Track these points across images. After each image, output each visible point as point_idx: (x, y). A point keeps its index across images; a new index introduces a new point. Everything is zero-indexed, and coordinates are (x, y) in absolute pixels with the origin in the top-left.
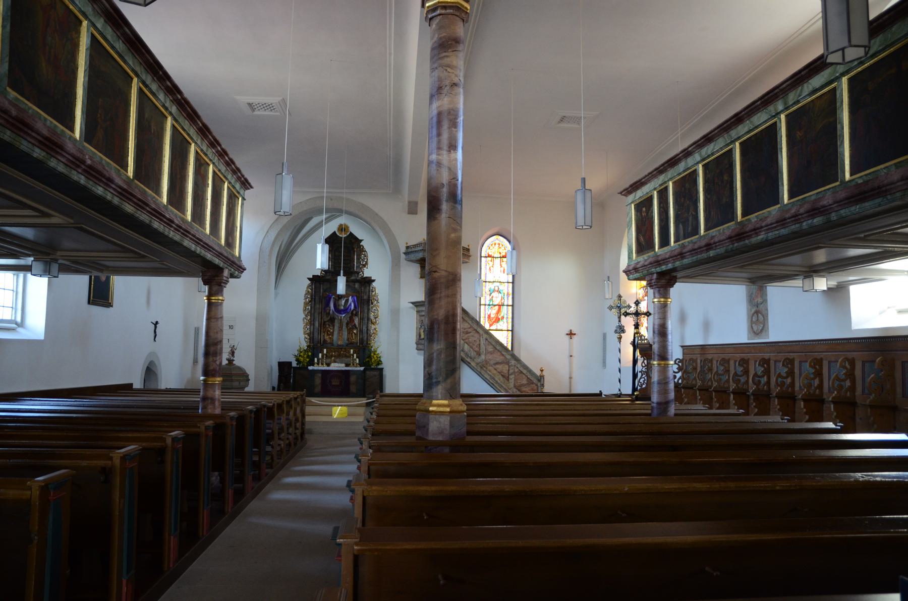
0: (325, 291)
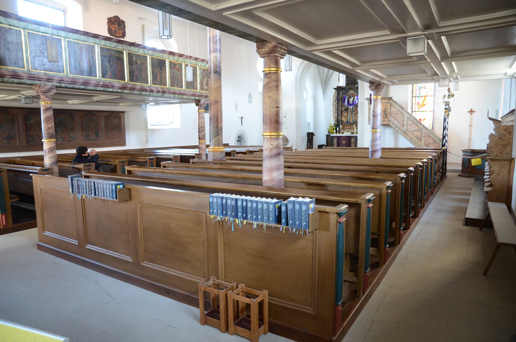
0: (343, 94)
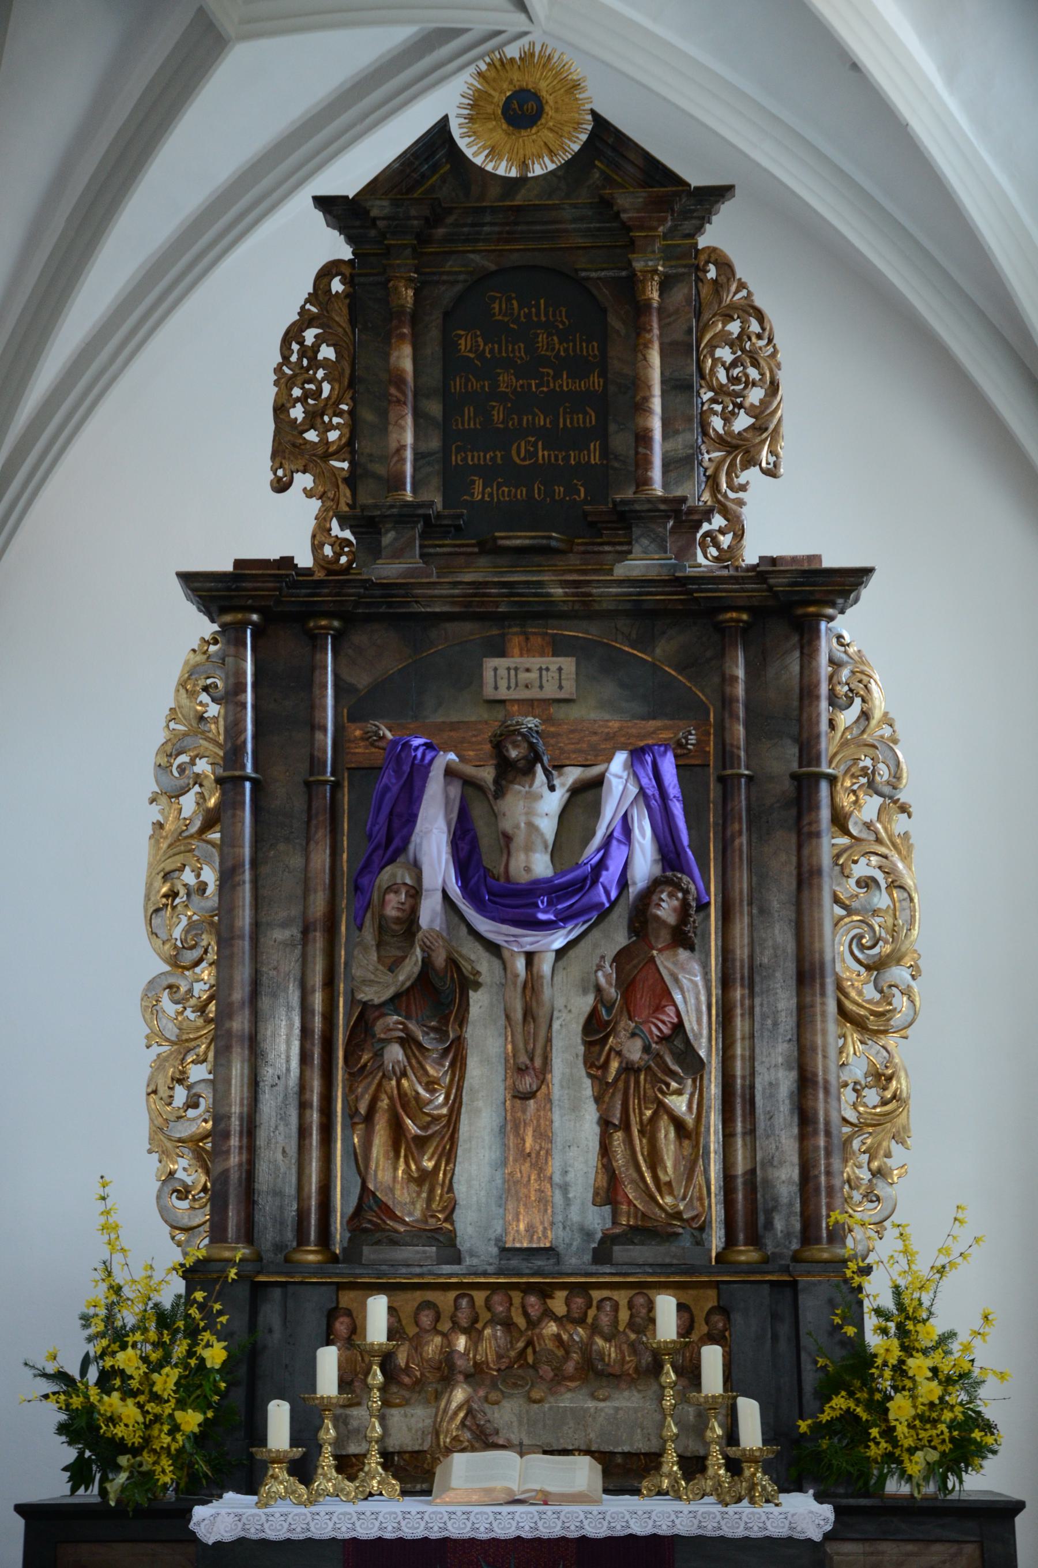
0: (356, 705)
